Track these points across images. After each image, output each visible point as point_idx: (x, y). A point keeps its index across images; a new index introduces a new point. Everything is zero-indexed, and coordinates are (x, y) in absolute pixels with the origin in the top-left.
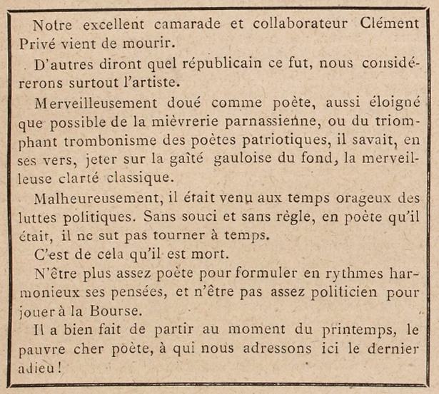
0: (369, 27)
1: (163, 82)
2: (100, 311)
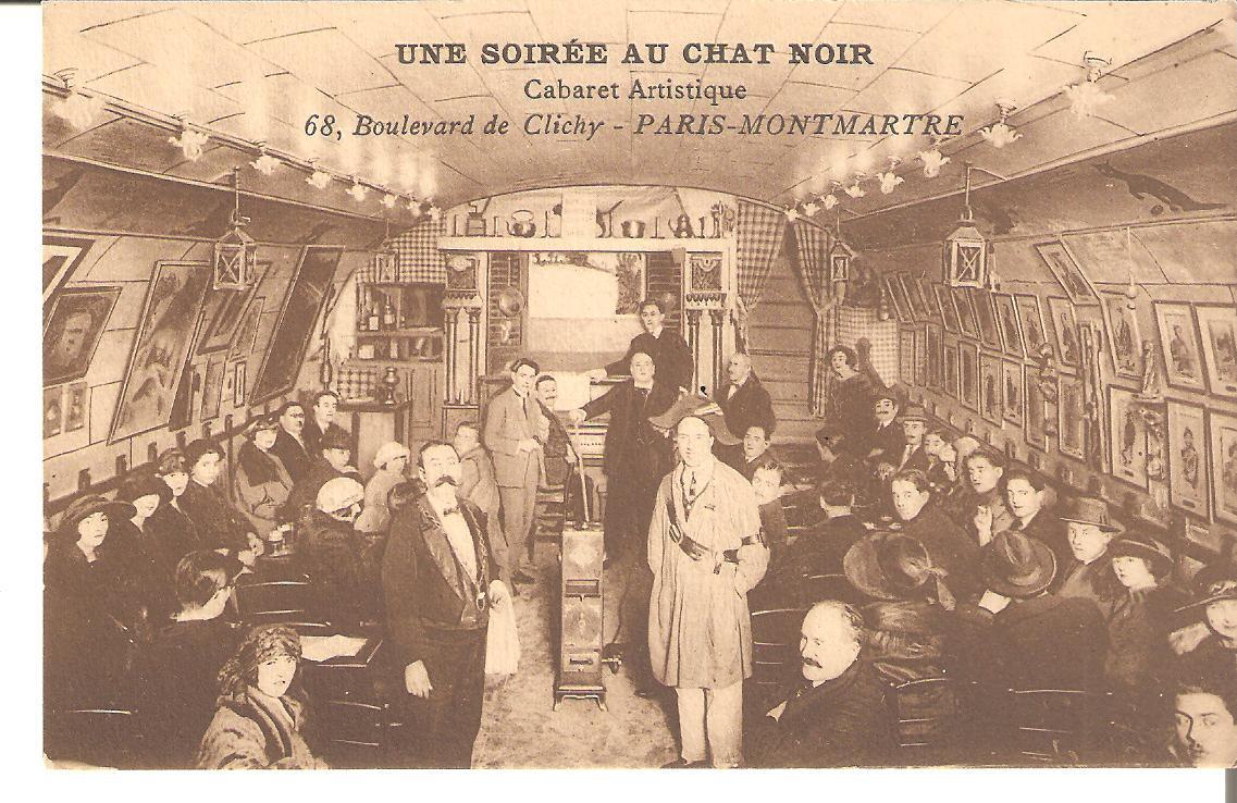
0: (539, 96)
1: (685, 91)
2: (372, 126)
